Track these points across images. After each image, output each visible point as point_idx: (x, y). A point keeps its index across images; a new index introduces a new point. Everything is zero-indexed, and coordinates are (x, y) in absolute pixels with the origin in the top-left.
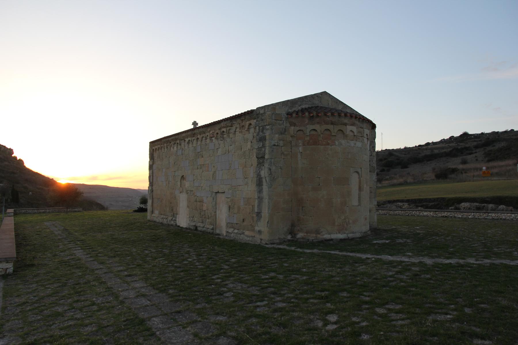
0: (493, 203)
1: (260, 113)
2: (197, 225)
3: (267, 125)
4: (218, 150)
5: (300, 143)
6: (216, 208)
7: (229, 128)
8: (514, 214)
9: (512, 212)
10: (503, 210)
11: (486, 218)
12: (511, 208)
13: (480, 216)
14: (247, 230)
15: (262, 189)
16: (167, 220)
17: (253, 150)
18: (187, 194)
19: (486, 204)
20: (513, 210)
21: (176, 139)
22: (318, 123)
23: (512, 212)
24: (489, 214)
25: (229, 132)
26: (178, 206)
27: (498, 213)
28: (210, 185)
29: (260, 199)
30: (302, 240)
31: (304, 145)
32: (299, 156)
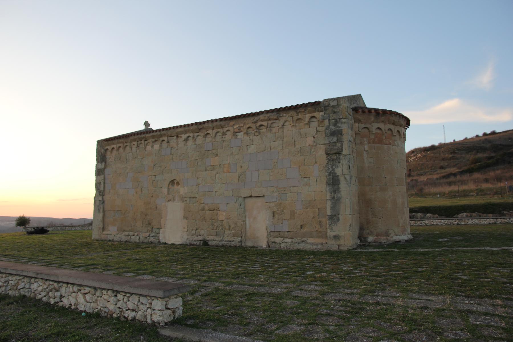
0: (421, 213)
1: (329, 104)
2: (206, 238)
3: (343, 118)
4: (248, 147)
5: (365, 141)
6: (245, 217)
7: (272, 121)
8: (443, 220)
9: (438, 219)
10: (430, 218)
11: (420, 224)
12: (436, 215)
13: (415, 223)
14: (309, 238)
15: (339, 188)
16: (138, 237)
17: (316, 145)
18: (183, 202)
19: (415, 214)
20: (438, 217)
21: (161, 136)
22: (383, 122)
23: (438, 219)
24: (423, 222)
25: (270, 127)
26: (162, 218)
27: (430, 220)
28: (233, 189)
29: (336, 201)
30: (374, 244)
31: (369, 143)
32: (365, 154)
